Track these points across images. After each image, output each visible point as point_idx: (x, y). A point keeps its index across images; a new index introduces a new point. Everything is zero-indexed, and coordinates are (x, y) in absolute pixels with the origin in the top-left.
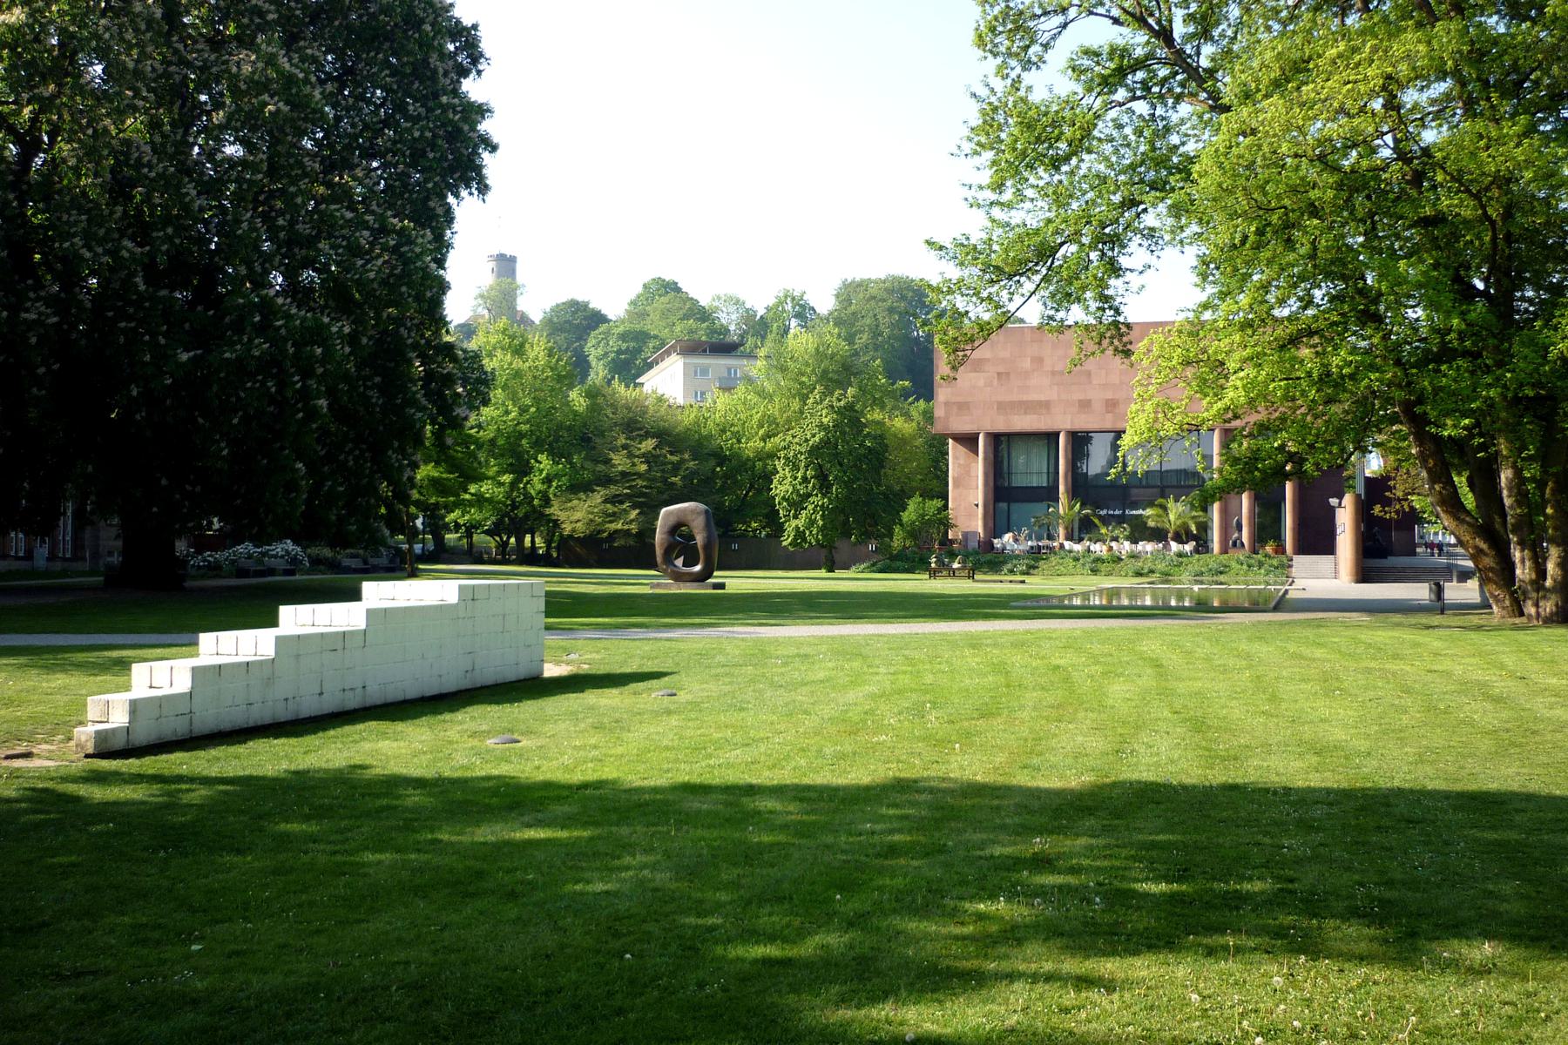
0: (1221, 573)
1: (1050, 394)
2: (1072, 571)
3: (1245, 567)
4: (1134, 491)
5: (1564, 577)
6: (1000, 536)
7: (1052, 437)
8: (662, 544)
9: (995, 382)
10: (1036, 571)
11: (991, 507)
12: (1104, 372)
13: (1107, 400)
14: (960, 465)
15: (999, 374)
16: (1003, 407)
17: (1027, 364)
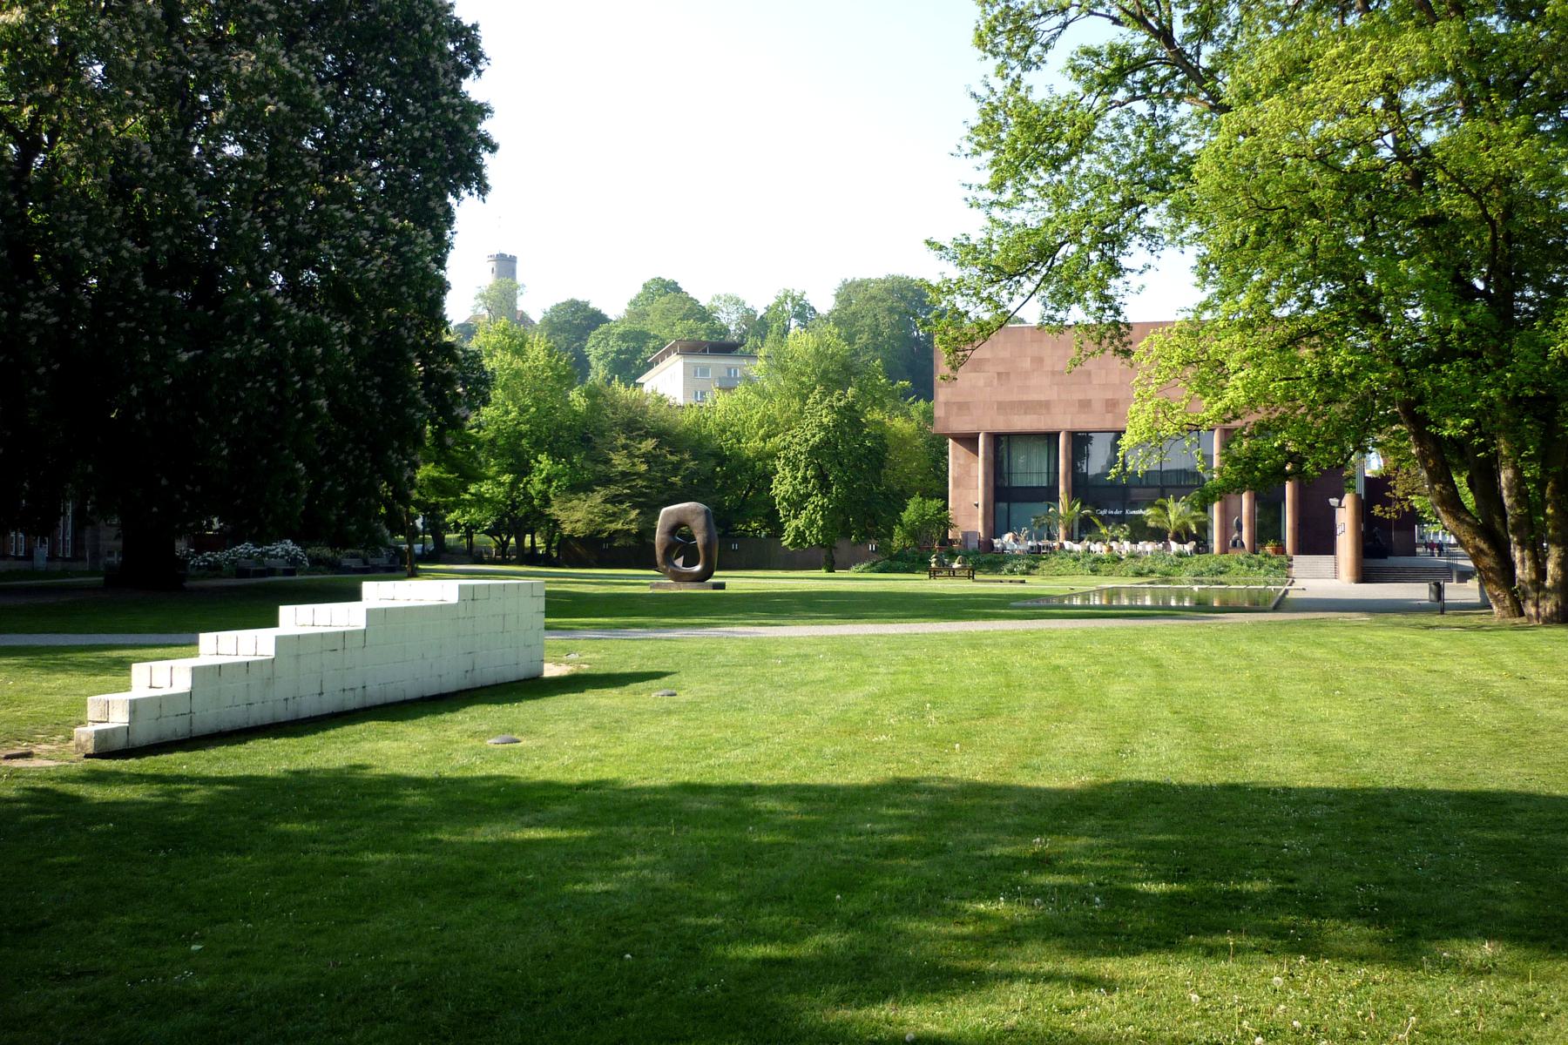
0: (1221, 573)
1: (1050, 394)
2: (1072, 571)
3: (1245, 567)
4: (1134, 491)
5: (1564, 577)
6: (1000, 536)
7: (1052, 437)
8: (662, 544)
9: (995, 382)
10: (1036, 571)
11: (991, 507)
12: (1104, 372)
13: (1107, 400)
14: (960, 465)
15: (999, 374)
16: (1003, 407)
17: (1027, 364)
